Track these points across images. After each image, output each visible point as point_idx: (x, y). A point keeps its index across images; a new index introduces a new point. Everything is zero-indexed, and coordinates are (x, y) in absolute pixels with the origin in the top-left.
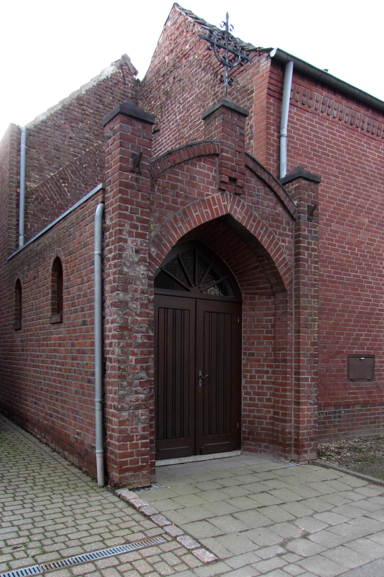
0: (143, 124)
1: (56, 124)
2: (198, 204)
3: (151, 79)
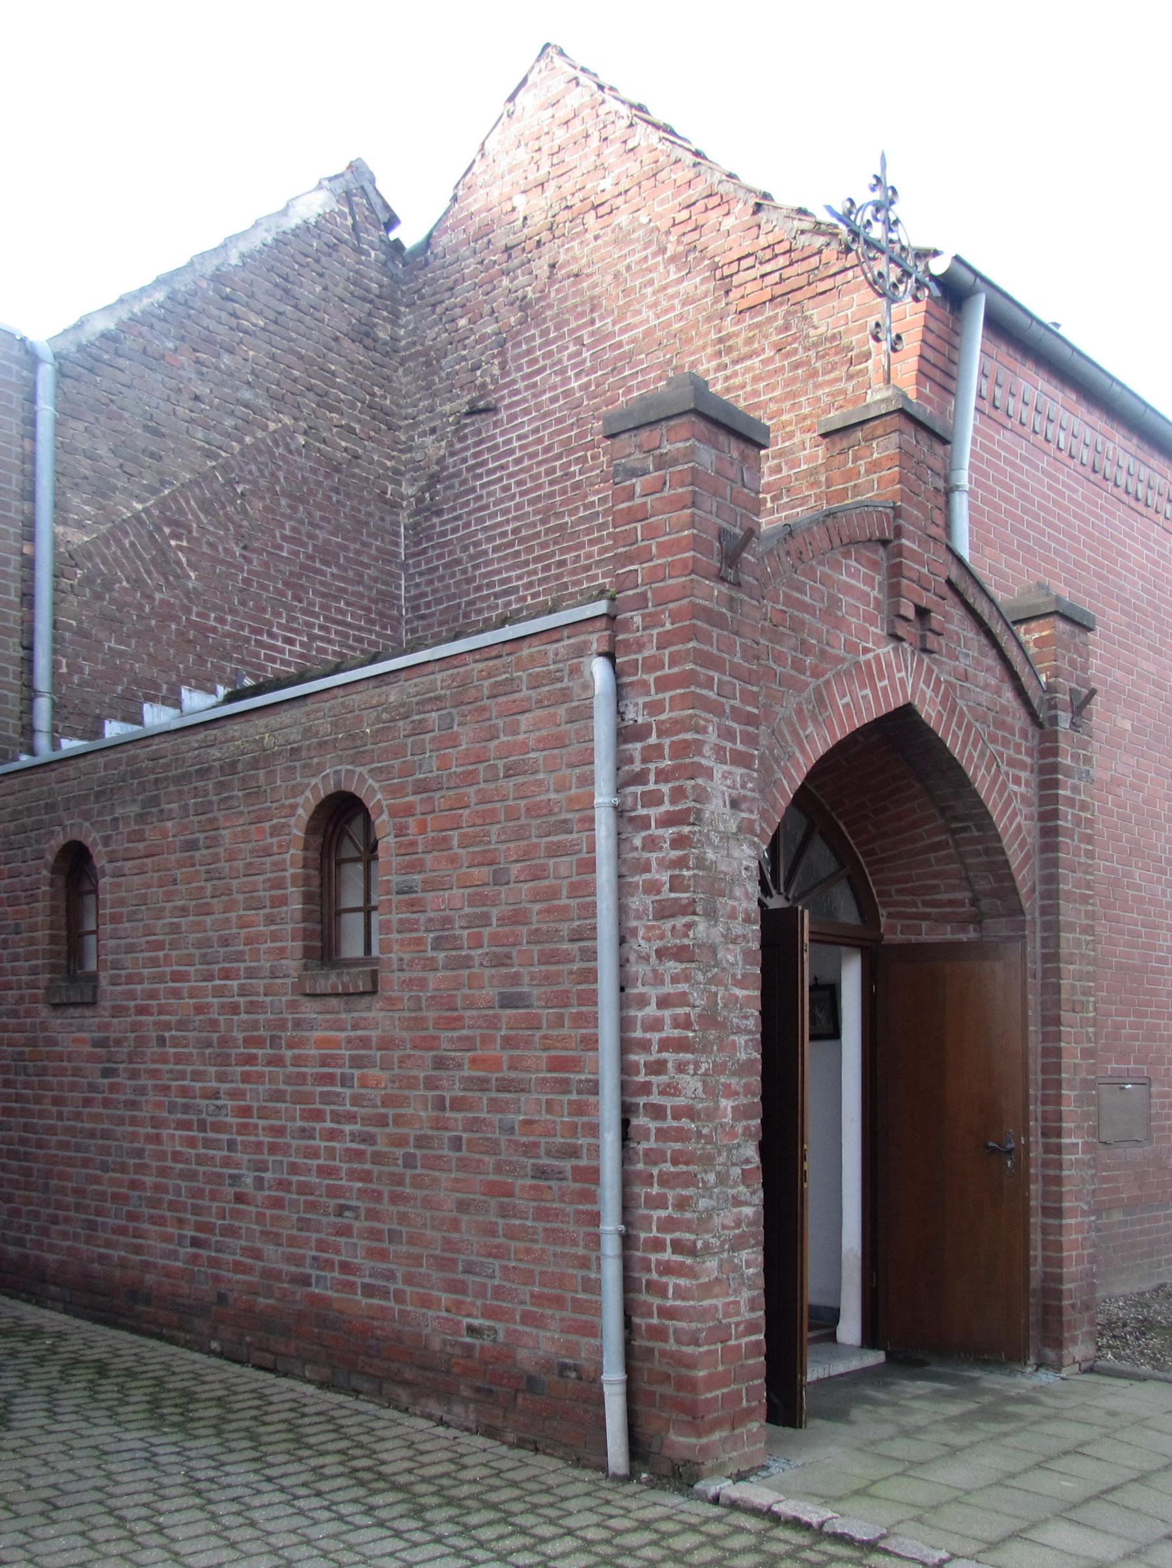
0: (742, 446)
1: (149, 349)
2: (848, 673)
3: (455, 250)
